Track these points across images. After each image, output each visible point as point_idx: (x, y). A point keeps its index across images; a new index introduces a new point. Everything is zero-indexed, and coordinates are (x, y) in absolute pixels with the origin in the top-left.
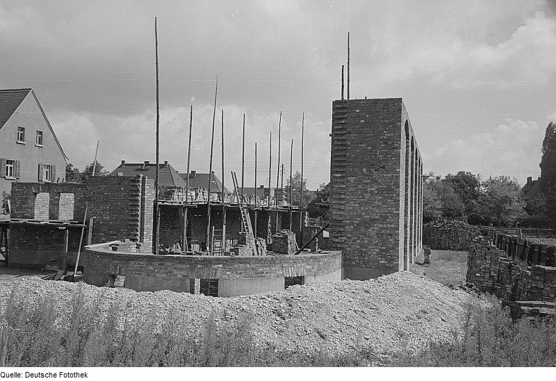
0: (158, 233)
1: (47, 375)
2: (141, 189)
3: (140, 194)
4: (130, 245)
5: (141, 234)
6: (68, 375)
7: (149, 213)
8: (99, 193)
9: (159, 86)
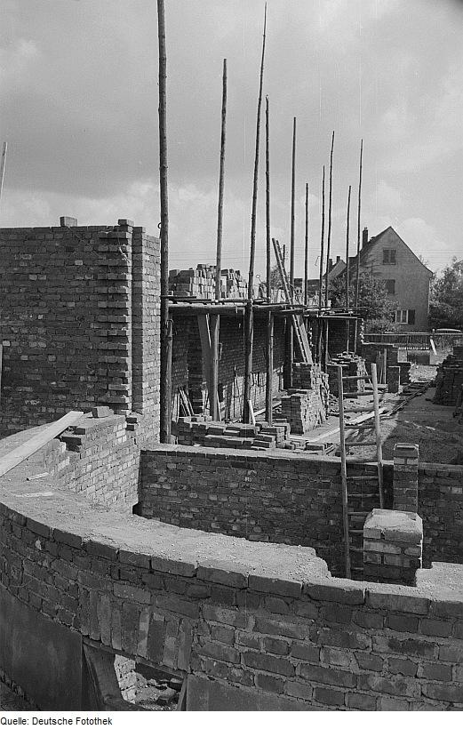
0: (169, 380)
1: (60, 722)
2: (130, 264)
3: (129, 277)
4: (112, 424)
6: (87, 721)
8: (15, 277)
9: (225, 145)
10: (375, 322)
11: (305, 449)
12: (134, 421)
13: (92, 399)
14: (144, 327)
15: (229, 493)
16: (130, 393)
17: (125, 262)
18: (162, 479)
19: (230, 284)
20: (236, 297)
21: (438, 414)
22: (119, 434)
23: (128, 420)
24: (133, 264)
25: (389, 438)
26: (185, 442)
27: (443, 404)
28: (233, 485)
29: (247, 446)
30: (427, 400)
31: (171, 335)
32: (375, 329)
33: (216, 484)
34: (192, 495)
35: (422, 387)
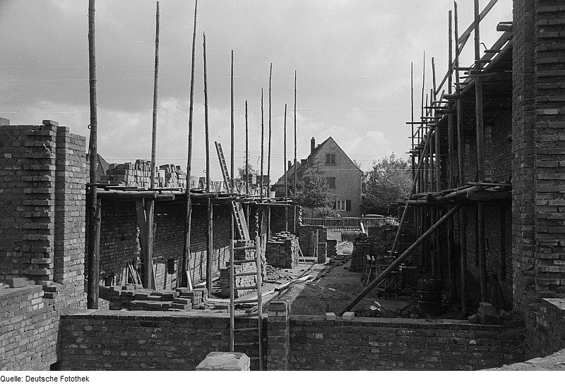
0: (97, 255)
1: (48, 379)
2: (53, 156)
3: (53, 168)
4: (25, 294)
5: (55, 262)
6: (69, 379)
7: (75, 211)
9: (159, 67)
10: (321, 209)
11: (214, 309)
12: (54, 290)
13: (17, 272)
14: (66, 210)
15: (138, 348)
16: (52, 266)
17: (48, 155)
18: (79, 340)
19: (168, 177)
20: (175, 186)
21: (350, 279)
22: (34, 302)
23: (45, 288)
24: (57, 157)
25: (298, 298)
26: (115, 308)
27: (356, 272)
28: (142, 342)
29: (165, 308)
30: (345, 268)
31: (99, 216)
32: (321, 215)
33: (126, 342)
34: (106, 352)
35: (344, 259)
